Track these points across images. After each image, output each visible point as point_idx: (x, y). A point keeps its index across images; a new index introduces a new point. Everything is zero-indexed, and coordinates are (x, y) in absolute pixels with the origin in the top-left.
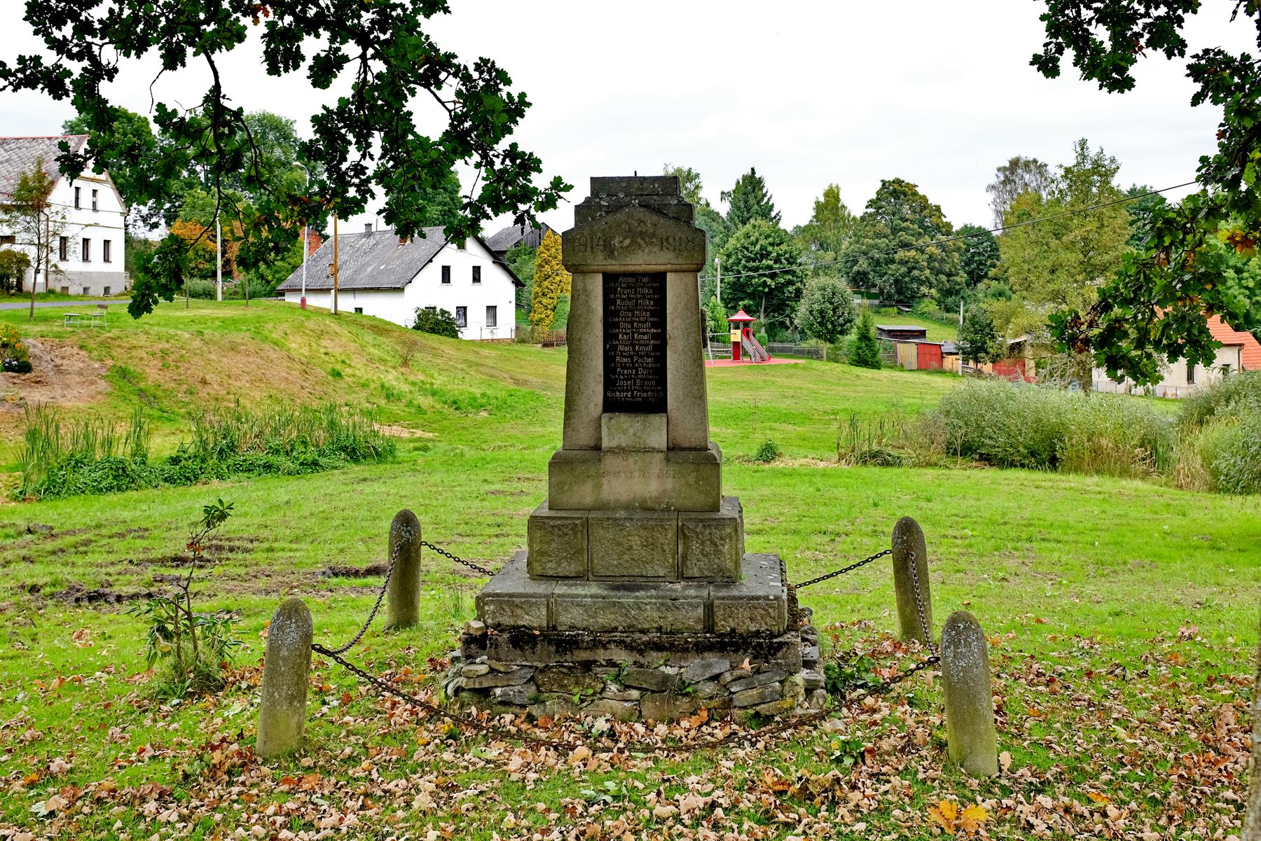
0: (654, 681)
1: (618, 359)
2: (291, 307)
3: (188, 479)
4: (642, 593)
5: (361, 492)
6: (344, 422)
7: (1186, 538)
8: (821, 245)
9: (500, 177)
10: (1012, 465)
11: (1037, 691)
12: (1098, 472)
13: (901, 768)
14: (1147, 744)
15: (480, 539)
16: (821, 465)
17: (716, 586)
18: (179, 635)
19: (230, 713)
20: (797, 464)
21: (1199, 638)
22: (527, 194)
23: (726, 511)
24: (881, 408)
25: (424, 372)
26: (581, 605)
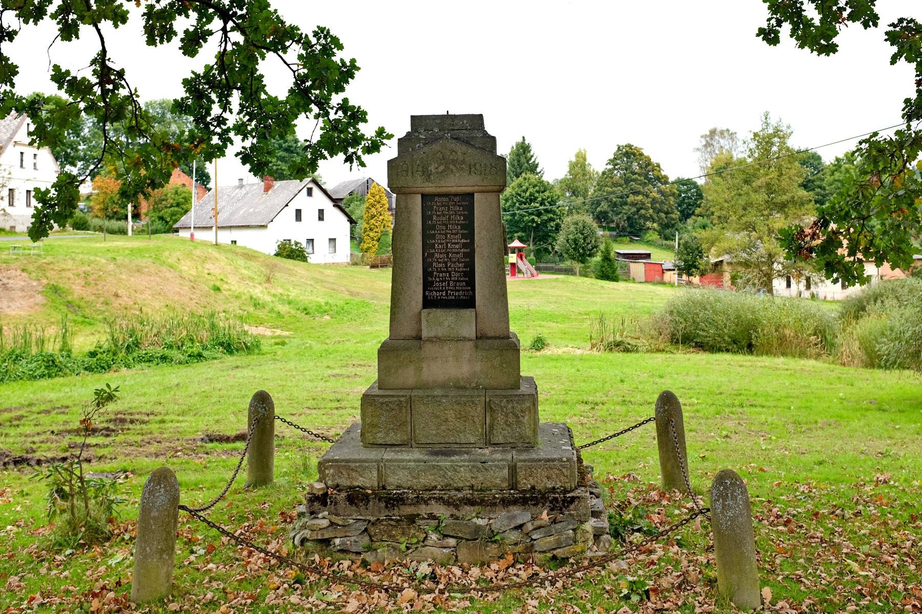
0: (467, 531)
2: (183, 240)
3: (103, 368)
4: (457, 457)
5: (234, 377)
6: (221, 324)
7: (857, 402)
8: (573, 193)
9: (334, 126)
10: (720, 350)
11: (777, 531)
12: (783, 354)
13: (680, 604)
14: (877, 576)
16: (579, 352)
17: (518, 451)
18: (73, 496)
19: (112, 562)
20: (560, 351)
21: (892, 483)
22: (357, 139)
23: (524, 389)
24: (620, 309)
25: (282, 287)
26: (406, 468)
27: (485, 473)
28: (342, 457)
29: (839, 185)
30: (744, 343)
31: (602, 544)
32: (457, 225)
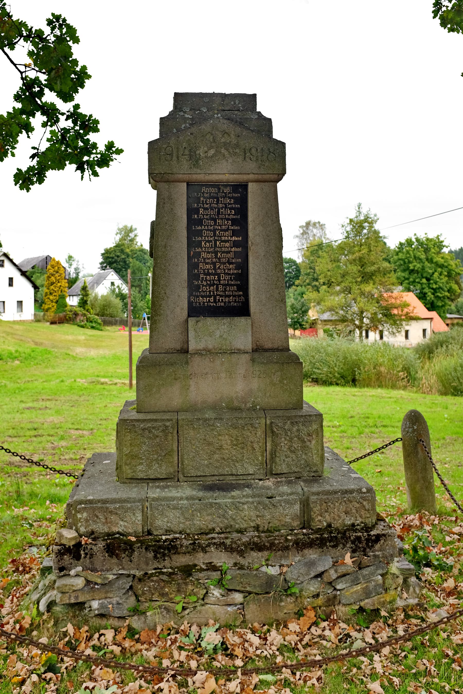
0: (257, 583)
1: (201, 265)
10: (331, 384)
15: (24, 439)
22: (90, 148)
26: (176, 509)
27: (273, 510)
28: (97, 497)
29: (402, 262)
30: (350, 378)
31: (411, 589)
32: (228, 219)
